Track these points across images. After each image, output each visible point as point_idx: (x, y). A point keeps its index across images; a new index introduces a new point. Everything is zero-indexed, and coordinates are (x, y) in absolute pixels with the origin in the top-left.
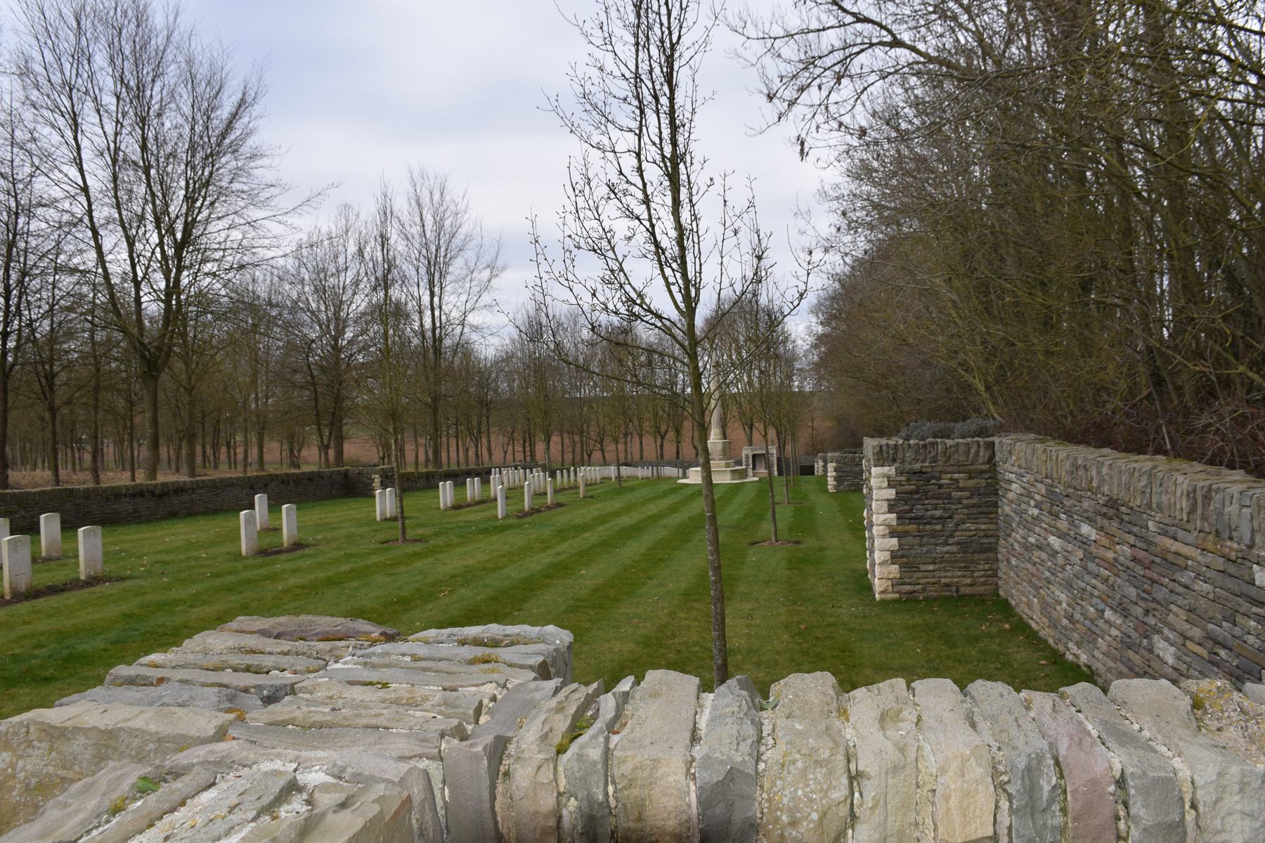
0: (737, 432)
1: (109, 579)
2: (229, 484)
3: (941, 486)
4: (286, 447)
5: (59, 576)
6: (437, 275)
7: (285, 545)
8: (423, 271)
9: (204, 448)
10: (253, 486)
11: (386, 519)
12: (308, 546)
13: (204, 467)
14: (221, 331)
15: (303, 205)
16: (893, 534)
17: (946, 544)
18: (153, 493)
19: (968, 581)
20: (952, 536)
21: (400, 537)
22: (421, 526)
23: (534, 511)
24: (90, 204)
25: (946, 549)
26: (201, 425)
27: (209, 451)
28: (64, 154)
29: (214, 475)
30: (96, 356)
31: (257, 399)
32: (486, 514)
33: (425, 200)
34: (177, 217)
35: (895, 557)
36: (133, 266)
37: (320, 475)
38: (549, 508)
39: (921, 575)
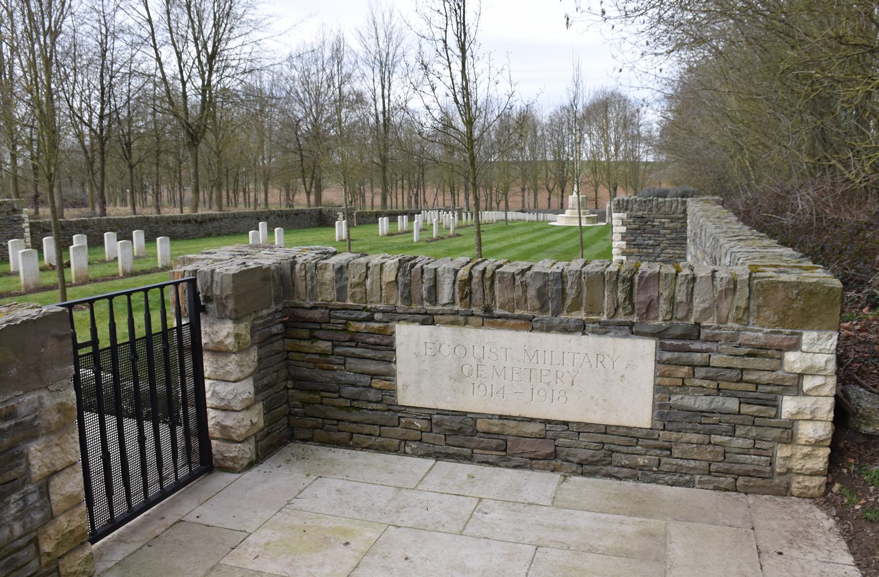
2: (243, 216)
3: (653, 226)
4: (284, 193)
5: (147, 266)
6: (387, 73)
8: (377, 70)
9: (228, 192)
10: (259, 217)
11: (342, 240)
13: (228, 206)
14: (238, 113)
18: (196, 221)
20: (659, 256)
22: (363, 244)
23: (439, 238)
26: (225, 177)
27: (231, 195)
29: (233, 210)
30: (158, 135)
31: (263, 158)
32: (408, 239)
33: (379, 20)
34: (209, 38)
36: (181, 72)
37: (303, 212)
38: (450, 237)
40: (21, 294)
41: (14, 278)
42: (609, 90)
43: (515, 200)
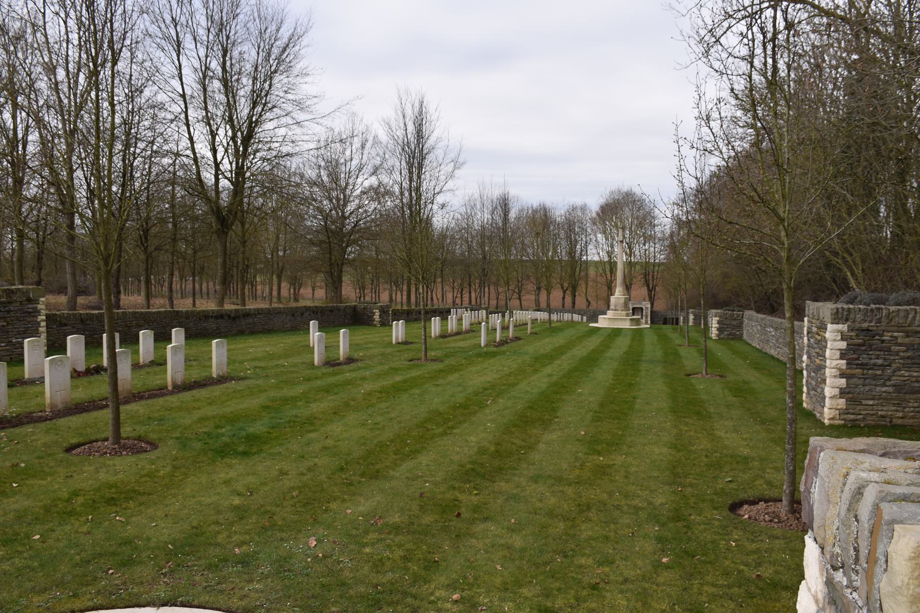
0: (640, 291)
1: (232, 379)
3: (883, 342)
7: (341, 359)
11: (399, 343)
12: (357, 360)
15: (336, 111)
16: (842, 375)
17: (884, 385)
18: (229, 316)
19: (900, 414)
20: (889, 380)
21: (423, 357)
24: (186, 107)
25: (884, 389)
28: (168, 69)
35: (843, 393)
39: (862, 407)
40: (46, 419)
41: (31, 390)
42: (625, 189)
43: (529, 298)
